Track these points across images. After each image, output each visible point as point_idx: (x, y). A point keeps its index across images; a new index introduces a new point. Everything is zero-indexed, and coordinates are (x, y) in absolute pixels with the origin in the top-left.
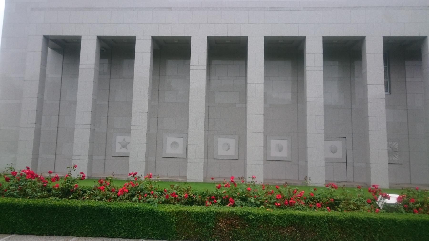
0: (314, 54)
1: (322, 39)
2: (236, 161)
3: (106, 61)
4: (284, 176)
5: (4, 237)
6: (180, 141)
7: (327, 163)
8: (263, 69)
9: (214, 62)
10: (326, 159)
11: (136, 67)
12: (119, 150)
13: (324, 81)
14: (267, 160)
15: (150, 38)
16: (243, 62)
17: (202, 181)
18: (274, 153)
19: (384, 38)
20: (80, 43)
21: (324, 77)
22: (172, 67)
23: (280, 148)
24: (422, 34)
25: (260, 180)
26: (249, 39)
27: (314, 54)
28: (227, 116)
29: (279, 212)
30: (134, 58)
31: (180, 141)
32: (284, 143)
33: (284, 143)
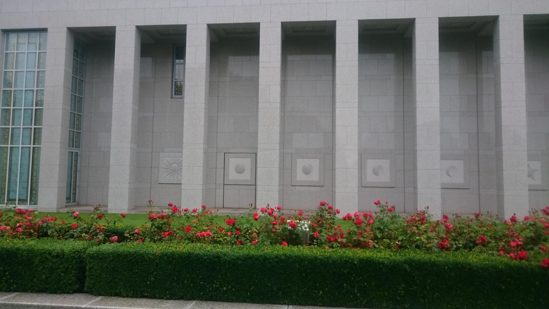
0: (426, 44)
1: (357, 24)
2: (467, 191)
3: (149, 60)
4: (464, 208)
5: (5, 295)
6: (246, 162)
7: (444, 190)
8: (357, 65)
9: (290, 58)
10: (442, 184)
11: (261, 65)
12: (164, 177)
13: (441, 79)
14: (362, 186)
15: (206, 26)
16: (329, 57)
17: (55, 211)
18: (371, 178)
19: (440, 19)
20: (185, 34)
21: (440, 74)
22: (236, 65)
23: (308, 170)
24: (491, 13)
25: (435, 215)
26: (337, 23)
27: (426, 44)
28: (310, 129)
29: (399, 257)
30: (259, 55)
31: (246, 162)
32: (385, 164)
33: (385, 164)
